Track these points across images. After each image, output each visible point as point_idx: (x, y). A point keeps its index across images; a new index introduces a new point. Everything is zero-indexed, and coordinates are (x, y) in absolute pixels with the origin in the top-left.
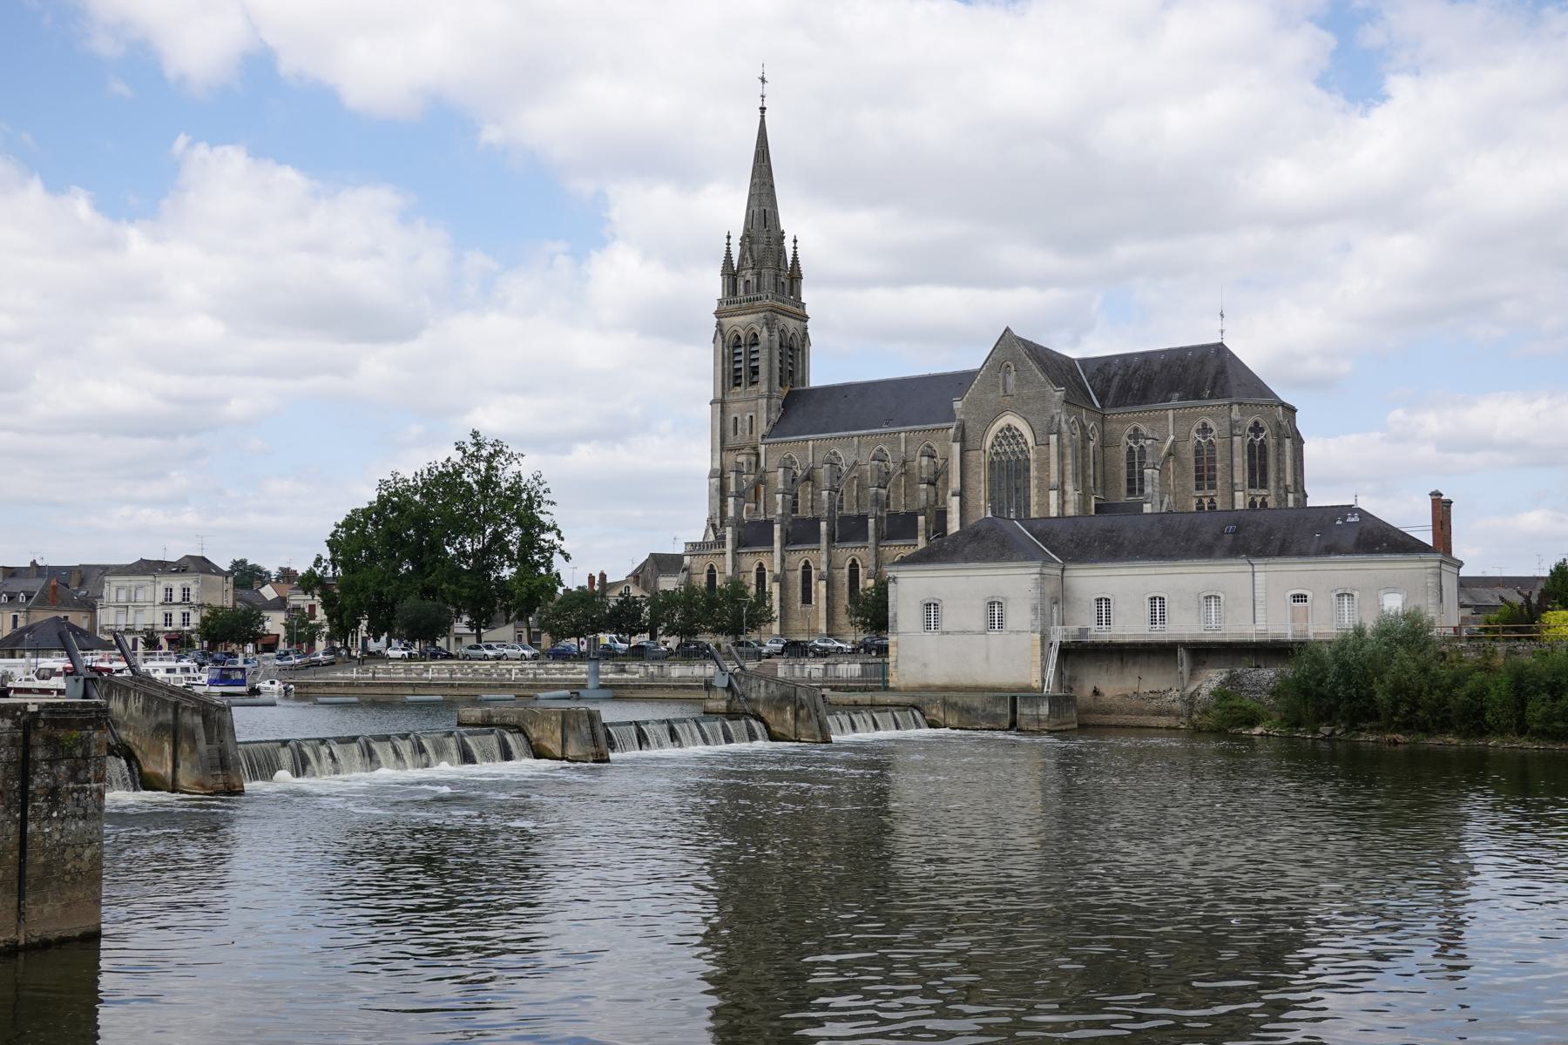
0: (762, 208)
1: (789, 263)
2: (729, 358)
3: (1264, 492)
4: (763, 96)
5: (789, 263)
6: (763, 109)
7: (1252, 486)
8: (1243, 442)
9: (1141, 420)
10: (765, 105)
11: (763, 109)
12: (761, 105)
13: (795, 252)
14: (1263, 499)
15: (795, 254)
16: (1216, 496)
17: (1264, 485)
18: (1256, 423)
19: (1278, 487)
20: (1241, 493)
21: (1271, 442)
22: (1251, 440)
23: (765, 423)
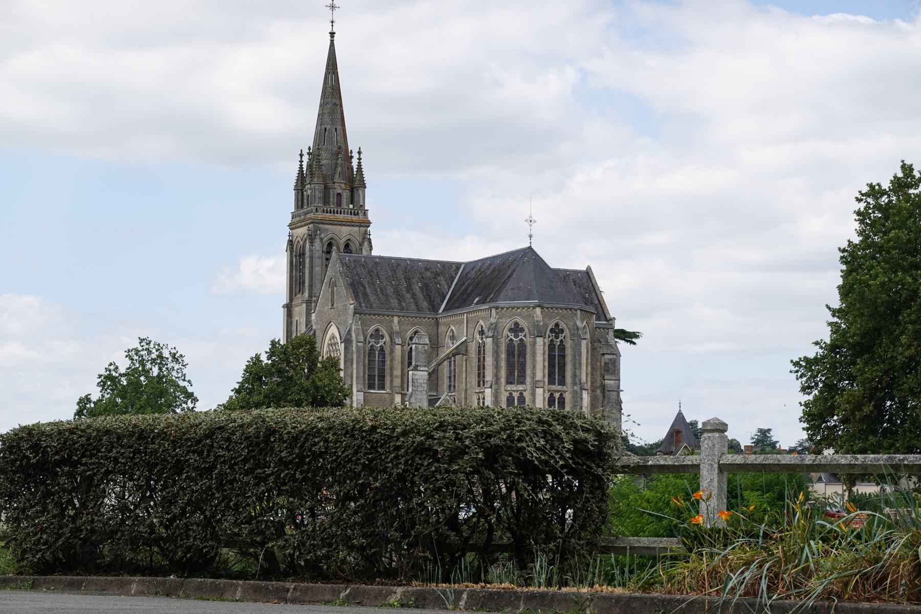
0: (323, 127)
1: (355, 170)
2: (296, 266)
3: (521, 387)
4: (332, 22)
5: (355, 170)
6: (332, 34)
7: (552, 381)
8: (402, 351)
9: (562, 319)
10: (334, 30)
11: (332, 34)
12: (330, 30)
13: (359, 163)
14: (561, 395)
15: (359, 165)
16: (525, 391)
17: (562, 382)
18: (557, 325)
19: (574, 383)
20: (542, 390)
21: (568, 344)
22: (552, 341)
23: (305, 326)
